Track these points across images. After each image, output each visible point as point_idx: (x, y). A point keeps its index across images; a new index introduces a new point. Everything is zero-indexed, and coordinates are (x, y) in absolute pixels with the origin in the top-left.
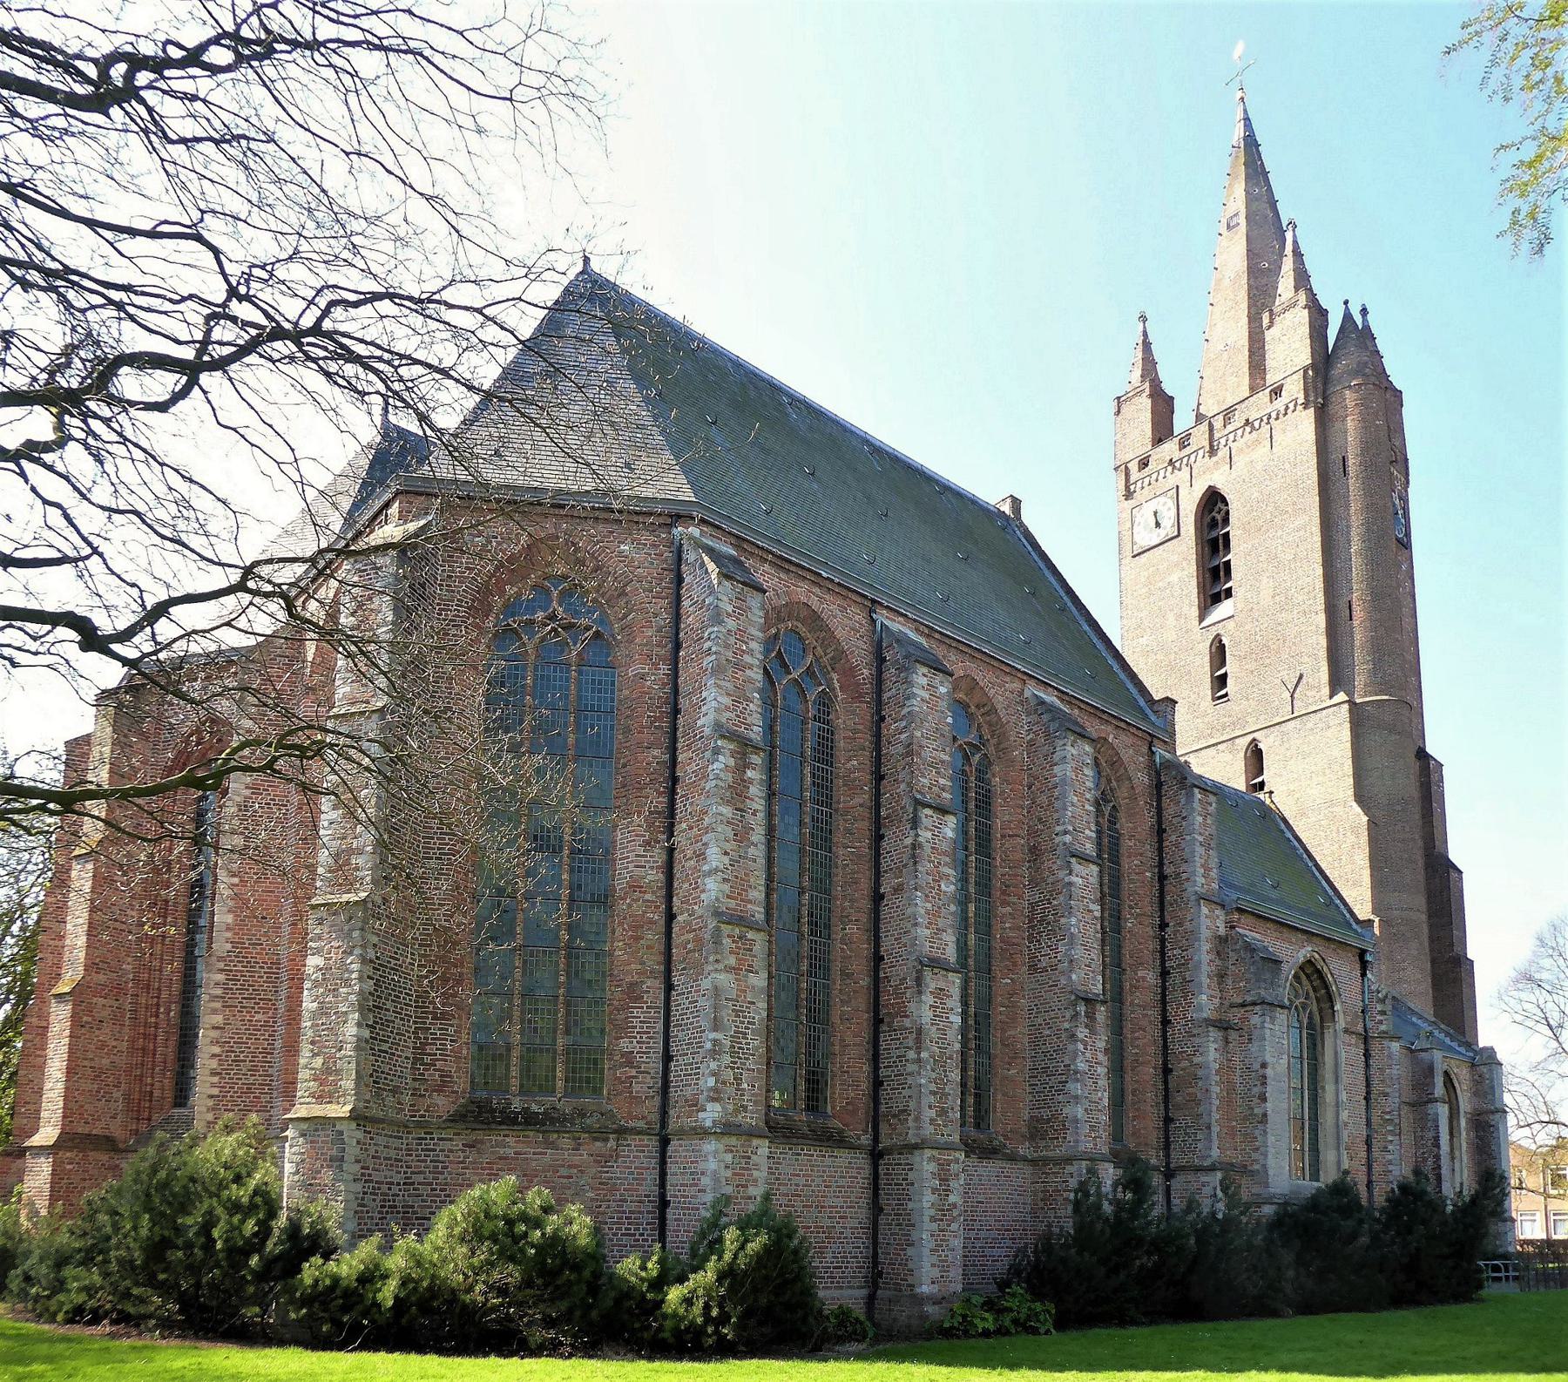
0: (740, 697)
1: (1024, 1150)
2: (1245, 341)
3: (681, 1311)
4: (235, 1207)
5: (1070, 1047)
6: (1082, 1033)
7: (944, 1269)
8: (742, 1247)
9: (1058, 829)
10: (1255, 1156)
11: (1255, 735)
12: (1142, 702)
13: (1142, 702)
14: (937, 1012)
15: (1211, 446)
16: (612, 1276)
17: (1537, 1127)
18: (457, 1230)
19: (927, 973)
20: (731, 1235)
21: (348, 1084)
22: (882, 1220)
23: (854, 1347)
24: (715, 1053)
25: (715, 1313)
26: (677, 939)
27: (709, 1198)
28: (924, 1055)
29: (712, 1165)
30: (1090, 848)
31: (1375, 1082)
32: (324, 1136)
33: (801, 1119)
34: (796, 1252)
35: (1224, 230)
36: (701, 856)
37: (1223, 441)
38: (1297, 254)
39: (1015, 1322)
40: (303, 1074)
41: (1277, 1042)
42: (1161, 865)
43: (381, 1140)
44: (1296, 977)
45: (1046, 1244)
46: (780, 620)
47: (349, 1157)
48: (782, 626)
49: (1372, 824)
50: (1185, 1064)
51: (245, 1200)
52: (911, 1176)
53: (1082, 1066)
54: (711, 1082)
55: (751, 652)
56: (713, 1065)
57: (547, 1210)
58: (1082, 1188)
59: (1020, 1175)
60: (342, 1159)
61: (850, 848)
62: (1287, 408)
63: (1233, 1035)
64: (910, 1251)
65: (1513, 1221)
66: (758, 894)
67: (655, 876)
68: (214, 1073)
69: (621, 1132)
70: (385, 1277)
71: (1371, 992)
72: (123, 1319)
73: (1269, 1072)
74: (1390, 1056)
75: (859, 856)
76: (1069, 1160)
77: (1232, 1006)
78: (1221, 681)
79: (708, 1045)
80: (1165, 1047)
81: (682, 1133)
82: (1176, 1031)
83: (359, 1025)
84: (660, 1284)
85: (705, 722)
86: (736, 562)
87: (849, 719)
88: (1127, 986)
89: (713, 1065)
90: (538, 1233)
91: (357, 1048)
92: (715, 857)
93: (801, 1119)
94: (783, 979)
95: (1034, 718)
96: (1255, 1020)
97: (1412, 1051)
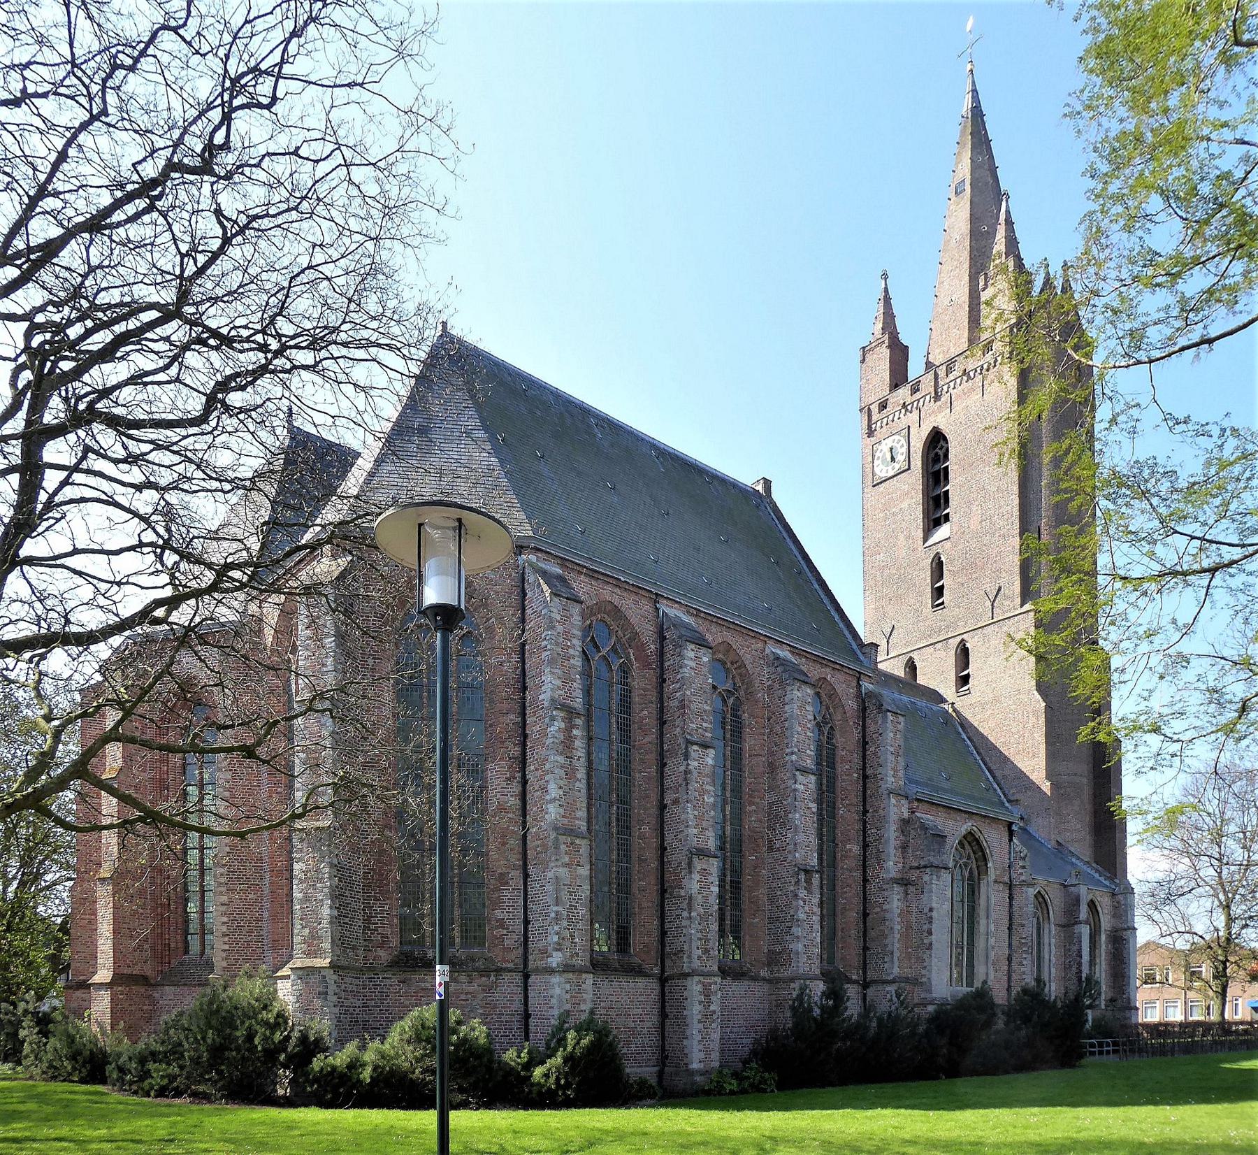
0: (567, 679)
1: (764, 973)
2: (966, 298)
3: (542, 1081)
4: (266, 1023)
6: (802, 893)
7: (708, 1053)
8: (578, 1043)
9: (788, 750)
10: (923, 972)
11: (965, 636)
12: (854, 646)
13: (854, 646)
14: (702, 886)
15: (936, 392)
16: (500, 1062)
17: (1176, 935)
18: (406, 1036)
19: (695, 859)
20: (571, 1035)
21: (326, 945)
22: (668, 1022)
23: (649, 1101)
24: (557, 919)
25: (562, 1082)
26: (530, 844)
27: (556, 1012)
29: (557, 991)
30: (810, 763)
32: (314, 979)
33: (614, 962)
34: (611, 1045)
35: (952, 195)
36: (544, 789)
37: (945, 388)
38: (1009, 223)
39: (752, 1085)
40: (296, 939)
41: (941, 895)
42: (864, 768)
43: (347, 980)
44: (961, 843)
45: (773, 1034)
46: (592, 614)
47: (330, 992)
48: (594, 618)
49: (1049, 709)
50: (878, 909)
51: (272, 1021)
52: (685, 994)
53: (802, 916)
54: (555, 938)
55: (573, 647)
56: (556, 928)
57: (459, 1023)
58: (800, 997)
60: (326, 993)
61: (643, 773)
62: (996, 361)
63: (911, 889)
64: (685, 1042)
65: (1137, 1009)
66: (582, 813)
67: (514, 802)
68: (225, 935)
69: (499, 971)
70: (364, 1065)
72: (195, 1095)
73: (934, 914)
74: (1027, 899)
75: (649, 779)
76: (793, 980)
77: (911, 868)
78: (939, 592)
79: (553, 915)
80: (865, 898)
81: (537, 971)
82: (873, 886)
83: (331, 908)
84: (529, 1066)
85: (545, 697)
86: (562, 579)
87: (641, 681)
89: (556, 928)
90: (455, 1037)
91: (331, 923)
92: (554, 791)
93: (614, 962)
94: (600, 865)
95: (772, 669)
96: (926, 878)
97: (1065, 886)
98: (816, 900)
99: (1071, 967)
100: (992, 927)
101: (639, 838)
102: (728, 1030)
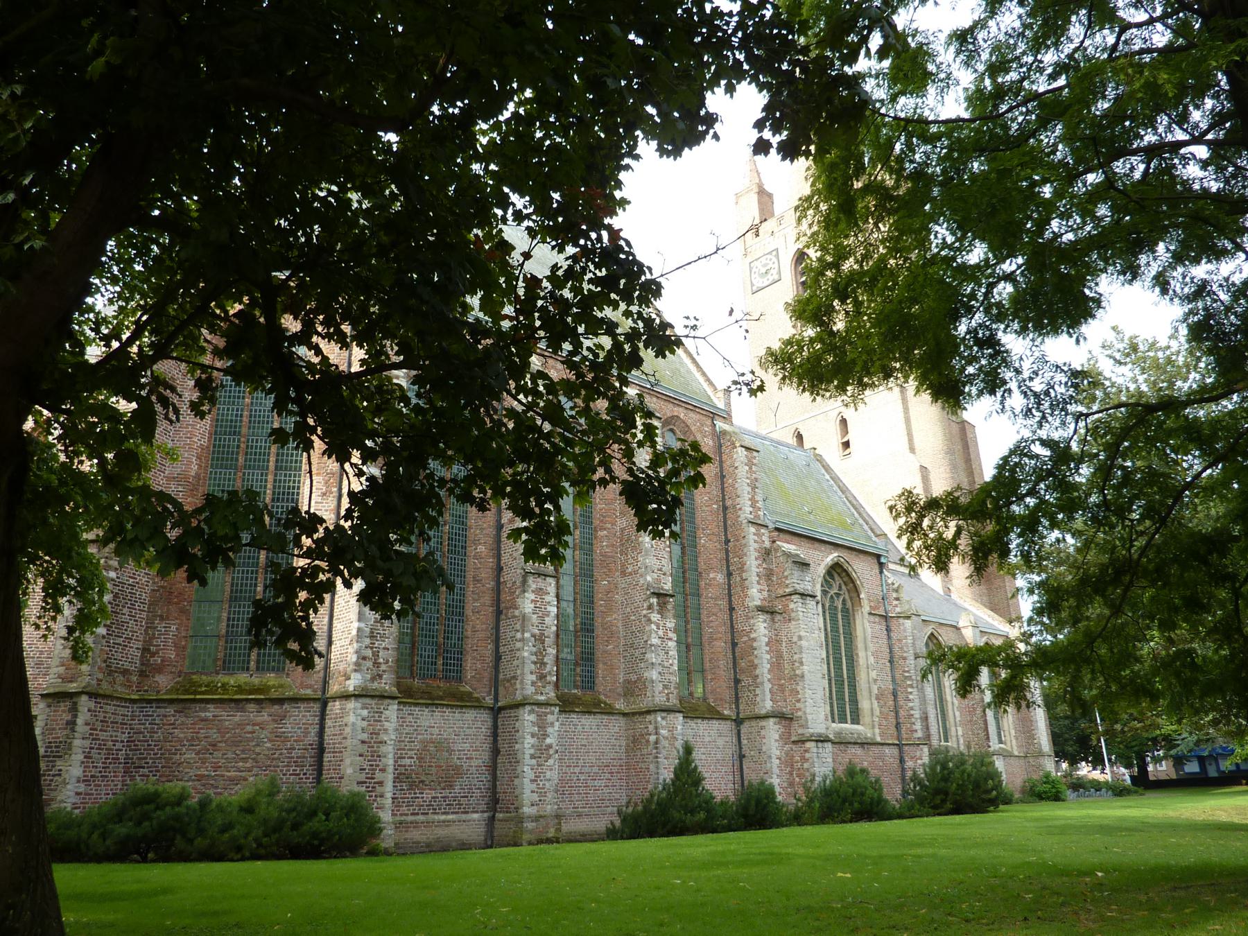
1: (620, 705)
5: (647, 628)
6: (655, 617)
10: (798, 705)
19: (531, 579)
28: (527, 635)
31: (896, 649)
41: (809, 625)
42: (724, 500)
50: (745, 639)
59: (616, 725)
63: (778, 617)
71: (888, 585)
82: (739, 612)
88: (702, 584)
96: (792, 606)
98: (671, 624)
99: (975, 709)
100: (872, 660)
101: (475, 557)
102: (577, 770)
